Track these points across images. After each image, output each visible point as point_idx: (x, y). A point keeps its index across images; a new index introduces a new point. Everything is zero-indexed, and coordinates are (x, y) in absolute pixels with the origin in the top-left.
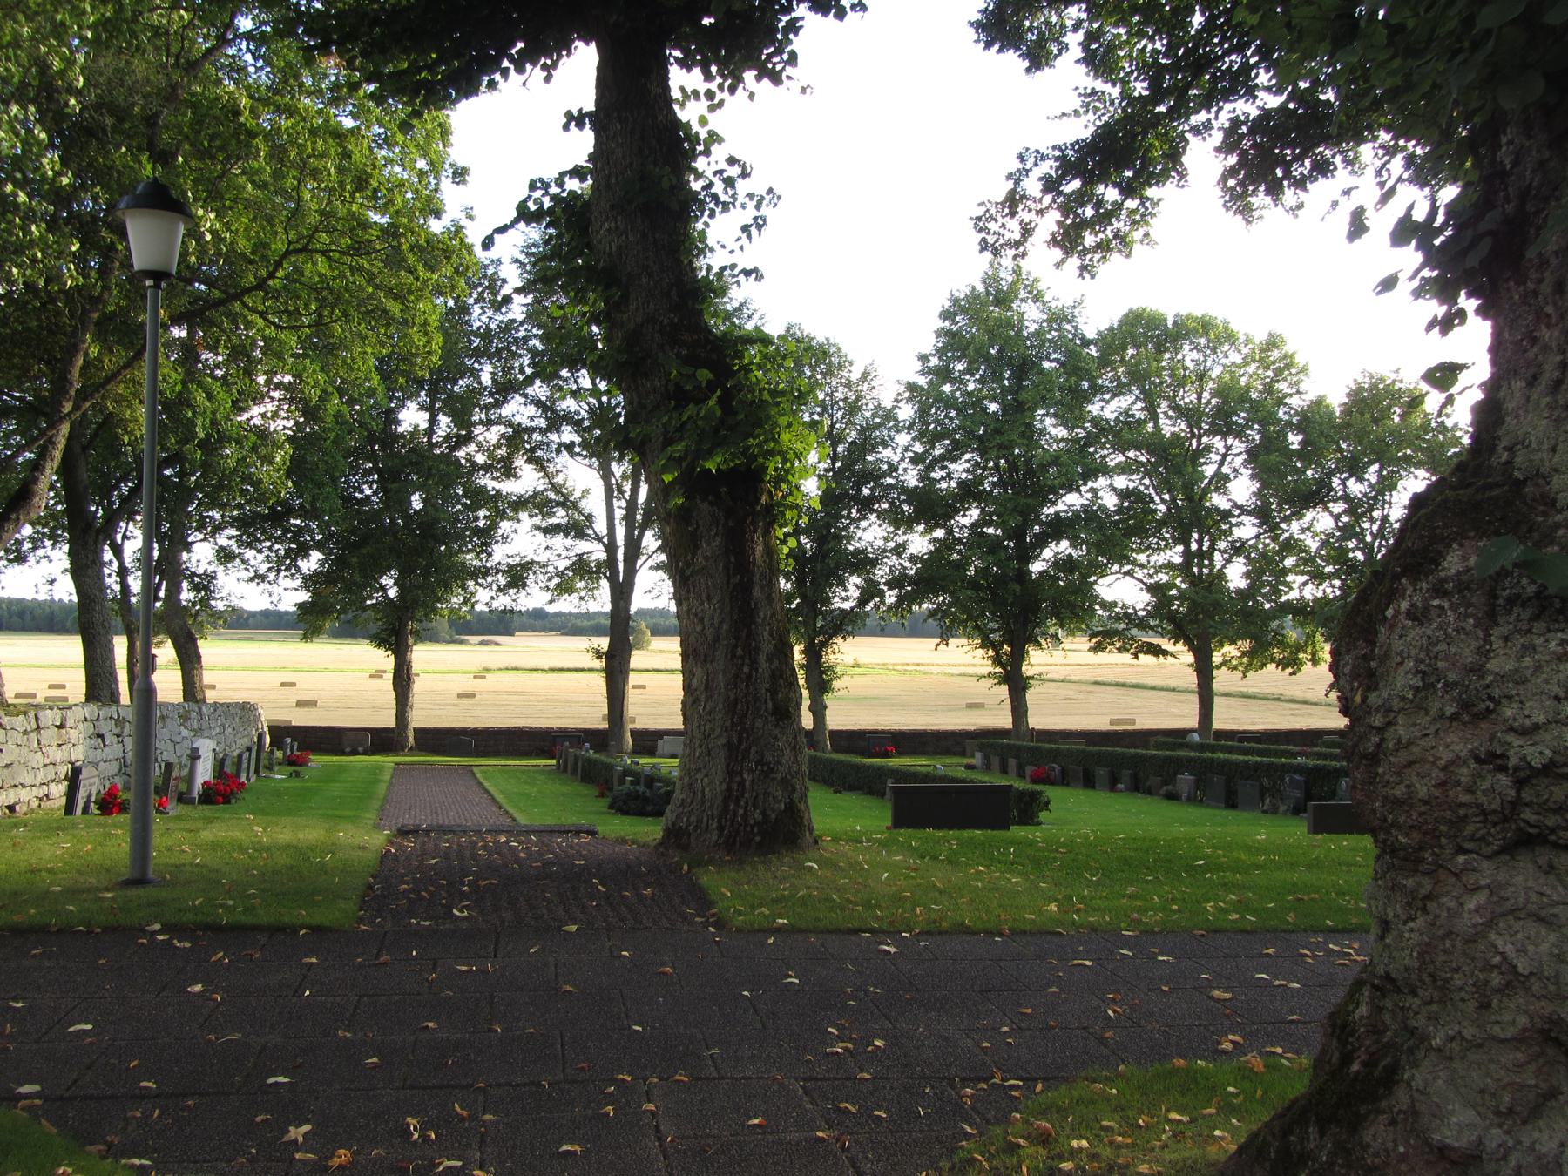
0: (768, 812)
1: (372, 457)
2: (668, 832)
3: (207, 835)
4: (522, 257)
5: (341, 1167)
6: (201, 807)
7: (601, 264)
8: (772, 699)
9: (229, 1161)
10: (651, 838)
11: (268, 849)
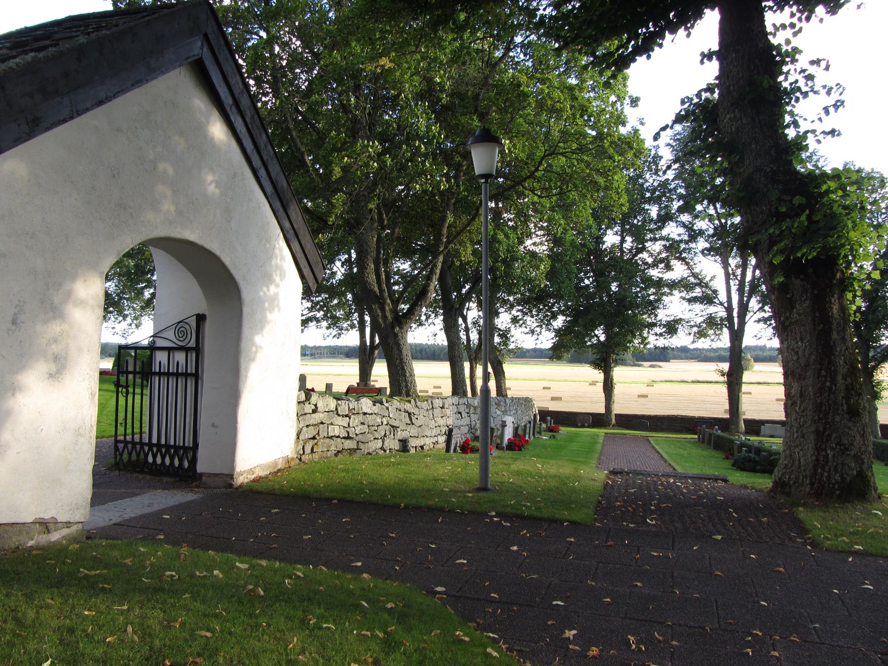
0: (845, 476)
1: (589, 263)
2: (776, 484)
3: (514, 467)
4: (671, 142)
5: (594, 657)
6: (507, 452)
7: (726, 139)
8: (847, 403)
9: (536, 643)
10: (764, 487)
11: (545, 477)
